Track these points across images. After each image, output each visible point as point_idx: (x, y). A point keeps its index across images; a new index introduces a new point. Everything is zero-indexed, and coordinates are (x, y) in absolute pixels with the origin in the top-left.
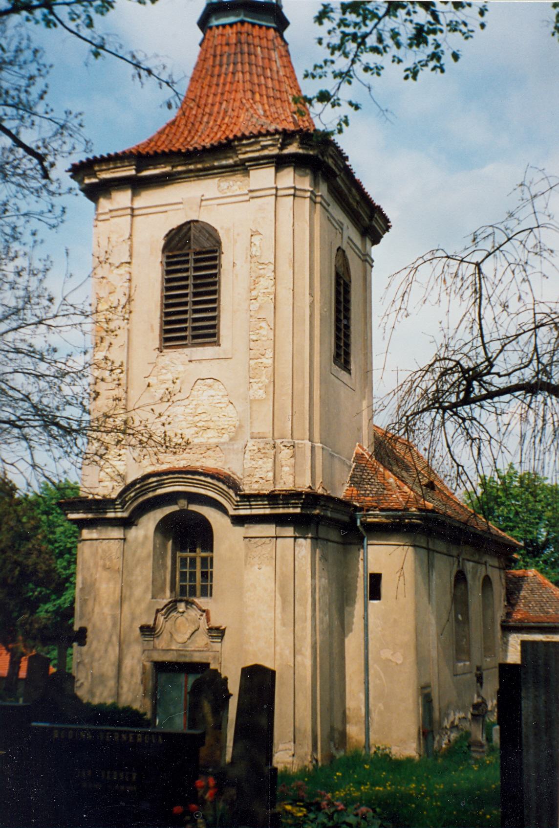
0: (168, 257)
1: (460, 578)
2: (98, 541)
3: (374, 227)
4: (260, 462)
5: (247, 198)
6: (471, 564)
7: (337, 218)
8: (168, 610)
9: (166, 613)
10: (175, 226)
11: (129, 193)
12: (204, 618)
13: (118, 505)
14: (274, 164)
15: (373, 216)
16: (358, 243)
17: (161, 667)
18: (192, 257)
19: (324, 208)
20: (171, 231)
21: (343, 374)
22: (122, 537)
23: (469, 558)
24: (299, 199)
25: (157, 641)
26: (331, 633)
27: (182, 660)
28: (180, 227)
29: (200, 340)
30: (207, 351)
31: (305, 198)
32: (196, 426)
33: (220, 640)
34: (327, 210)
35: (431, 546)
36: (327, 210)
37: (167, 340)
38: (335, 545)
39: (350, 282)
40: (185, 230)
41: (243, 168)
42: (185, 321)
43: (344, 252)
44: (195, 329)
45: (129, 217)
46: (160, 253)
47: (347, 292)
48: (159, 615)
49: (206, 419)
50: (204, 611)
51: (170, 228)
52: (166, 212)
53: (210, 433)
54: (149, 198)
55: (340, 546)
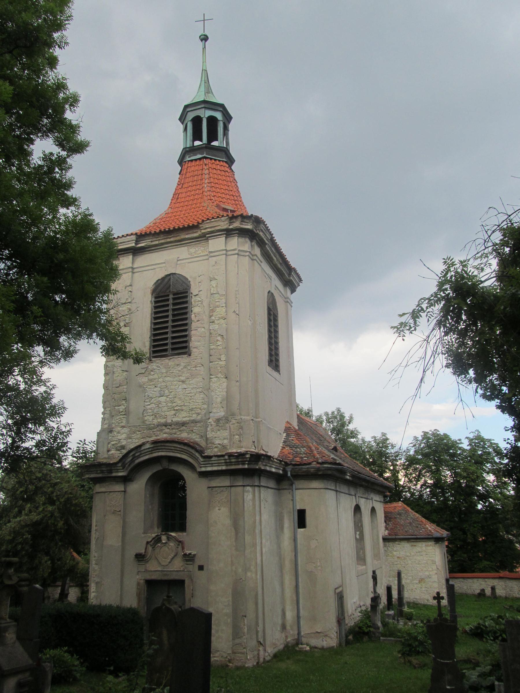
0: (156, 298)
1: (357, 509)
2: (106, 494)
3: (292, 280)
4: (218, 433)
5: (206, 257)
6: (364, 500)
7: (268, 272)
8: (155, 542)
9: (153, 544)
10: (160, 278)
11: (131, 257)
12: (180, 547)
13: (120, 466)
14: (225, 236)
15: (291, 274)
16: (282, 291)
17: (151, 584)
18: (171, 296)
19: (259, 264)
20: (158, 281)
21: (275, 374)
22: (123, 490)
23: (361, 496)
24: (242, 257)
25: (147, 565)
26: (258, 242)
27: (166, 578)
28: (163, 279)
29: (176, 352)
30: (182, 360)
31: (246, 256)
32: (174, 410)
33: (192, 563)
34: (260, 265)
35: (338, 489)
36: (260, 265)
37: (154, 352)
38: (273, 490)
39: (278, 314)
40: (166, 280)
41: (205, 237)
42: (166, 339)
43: (272, 294)
44: (173, 344)
45: (131, 273)
46: (150, 296)
47: (276, 319)
48: (149, 546)
49: (181, 404)
50: (180, 542)
51: (157, 279)
52: (155, 269)
53: (184, 414)
54: (143, 260)
55: (276, 491)
